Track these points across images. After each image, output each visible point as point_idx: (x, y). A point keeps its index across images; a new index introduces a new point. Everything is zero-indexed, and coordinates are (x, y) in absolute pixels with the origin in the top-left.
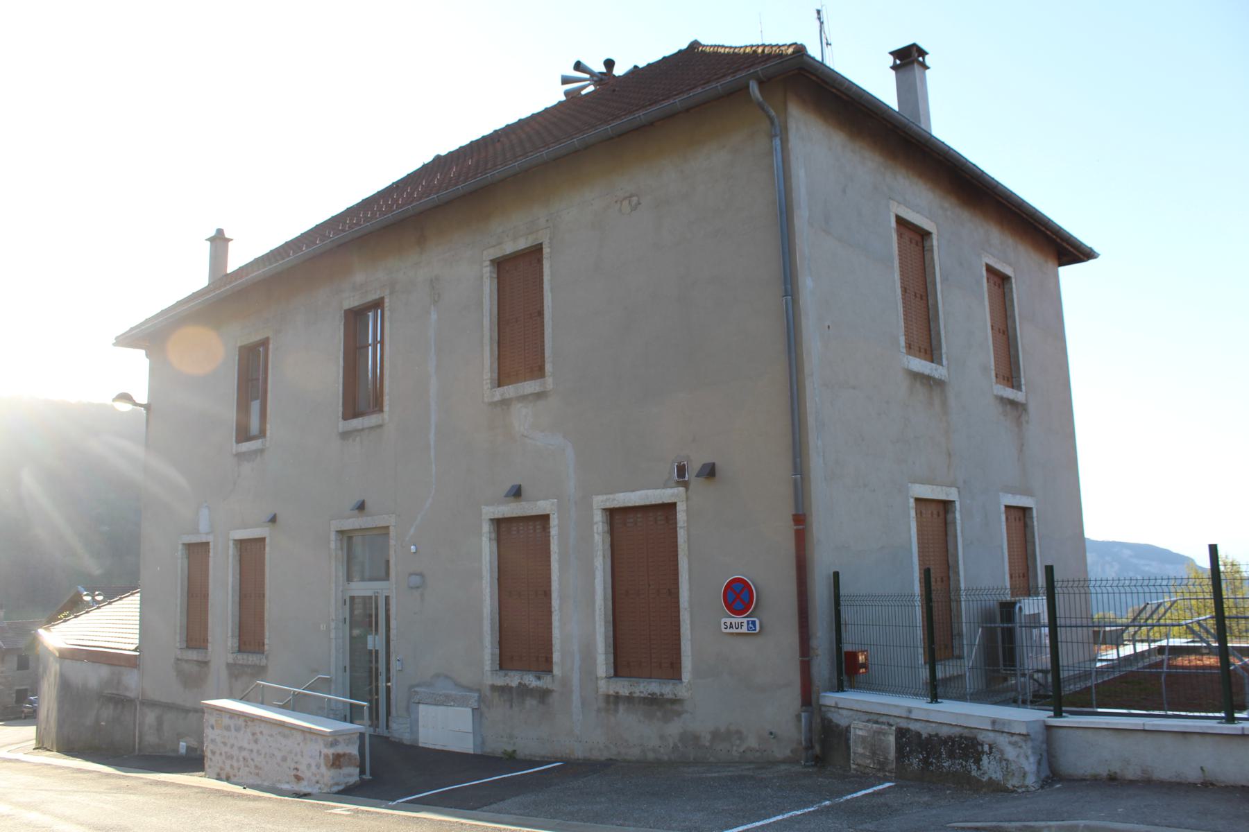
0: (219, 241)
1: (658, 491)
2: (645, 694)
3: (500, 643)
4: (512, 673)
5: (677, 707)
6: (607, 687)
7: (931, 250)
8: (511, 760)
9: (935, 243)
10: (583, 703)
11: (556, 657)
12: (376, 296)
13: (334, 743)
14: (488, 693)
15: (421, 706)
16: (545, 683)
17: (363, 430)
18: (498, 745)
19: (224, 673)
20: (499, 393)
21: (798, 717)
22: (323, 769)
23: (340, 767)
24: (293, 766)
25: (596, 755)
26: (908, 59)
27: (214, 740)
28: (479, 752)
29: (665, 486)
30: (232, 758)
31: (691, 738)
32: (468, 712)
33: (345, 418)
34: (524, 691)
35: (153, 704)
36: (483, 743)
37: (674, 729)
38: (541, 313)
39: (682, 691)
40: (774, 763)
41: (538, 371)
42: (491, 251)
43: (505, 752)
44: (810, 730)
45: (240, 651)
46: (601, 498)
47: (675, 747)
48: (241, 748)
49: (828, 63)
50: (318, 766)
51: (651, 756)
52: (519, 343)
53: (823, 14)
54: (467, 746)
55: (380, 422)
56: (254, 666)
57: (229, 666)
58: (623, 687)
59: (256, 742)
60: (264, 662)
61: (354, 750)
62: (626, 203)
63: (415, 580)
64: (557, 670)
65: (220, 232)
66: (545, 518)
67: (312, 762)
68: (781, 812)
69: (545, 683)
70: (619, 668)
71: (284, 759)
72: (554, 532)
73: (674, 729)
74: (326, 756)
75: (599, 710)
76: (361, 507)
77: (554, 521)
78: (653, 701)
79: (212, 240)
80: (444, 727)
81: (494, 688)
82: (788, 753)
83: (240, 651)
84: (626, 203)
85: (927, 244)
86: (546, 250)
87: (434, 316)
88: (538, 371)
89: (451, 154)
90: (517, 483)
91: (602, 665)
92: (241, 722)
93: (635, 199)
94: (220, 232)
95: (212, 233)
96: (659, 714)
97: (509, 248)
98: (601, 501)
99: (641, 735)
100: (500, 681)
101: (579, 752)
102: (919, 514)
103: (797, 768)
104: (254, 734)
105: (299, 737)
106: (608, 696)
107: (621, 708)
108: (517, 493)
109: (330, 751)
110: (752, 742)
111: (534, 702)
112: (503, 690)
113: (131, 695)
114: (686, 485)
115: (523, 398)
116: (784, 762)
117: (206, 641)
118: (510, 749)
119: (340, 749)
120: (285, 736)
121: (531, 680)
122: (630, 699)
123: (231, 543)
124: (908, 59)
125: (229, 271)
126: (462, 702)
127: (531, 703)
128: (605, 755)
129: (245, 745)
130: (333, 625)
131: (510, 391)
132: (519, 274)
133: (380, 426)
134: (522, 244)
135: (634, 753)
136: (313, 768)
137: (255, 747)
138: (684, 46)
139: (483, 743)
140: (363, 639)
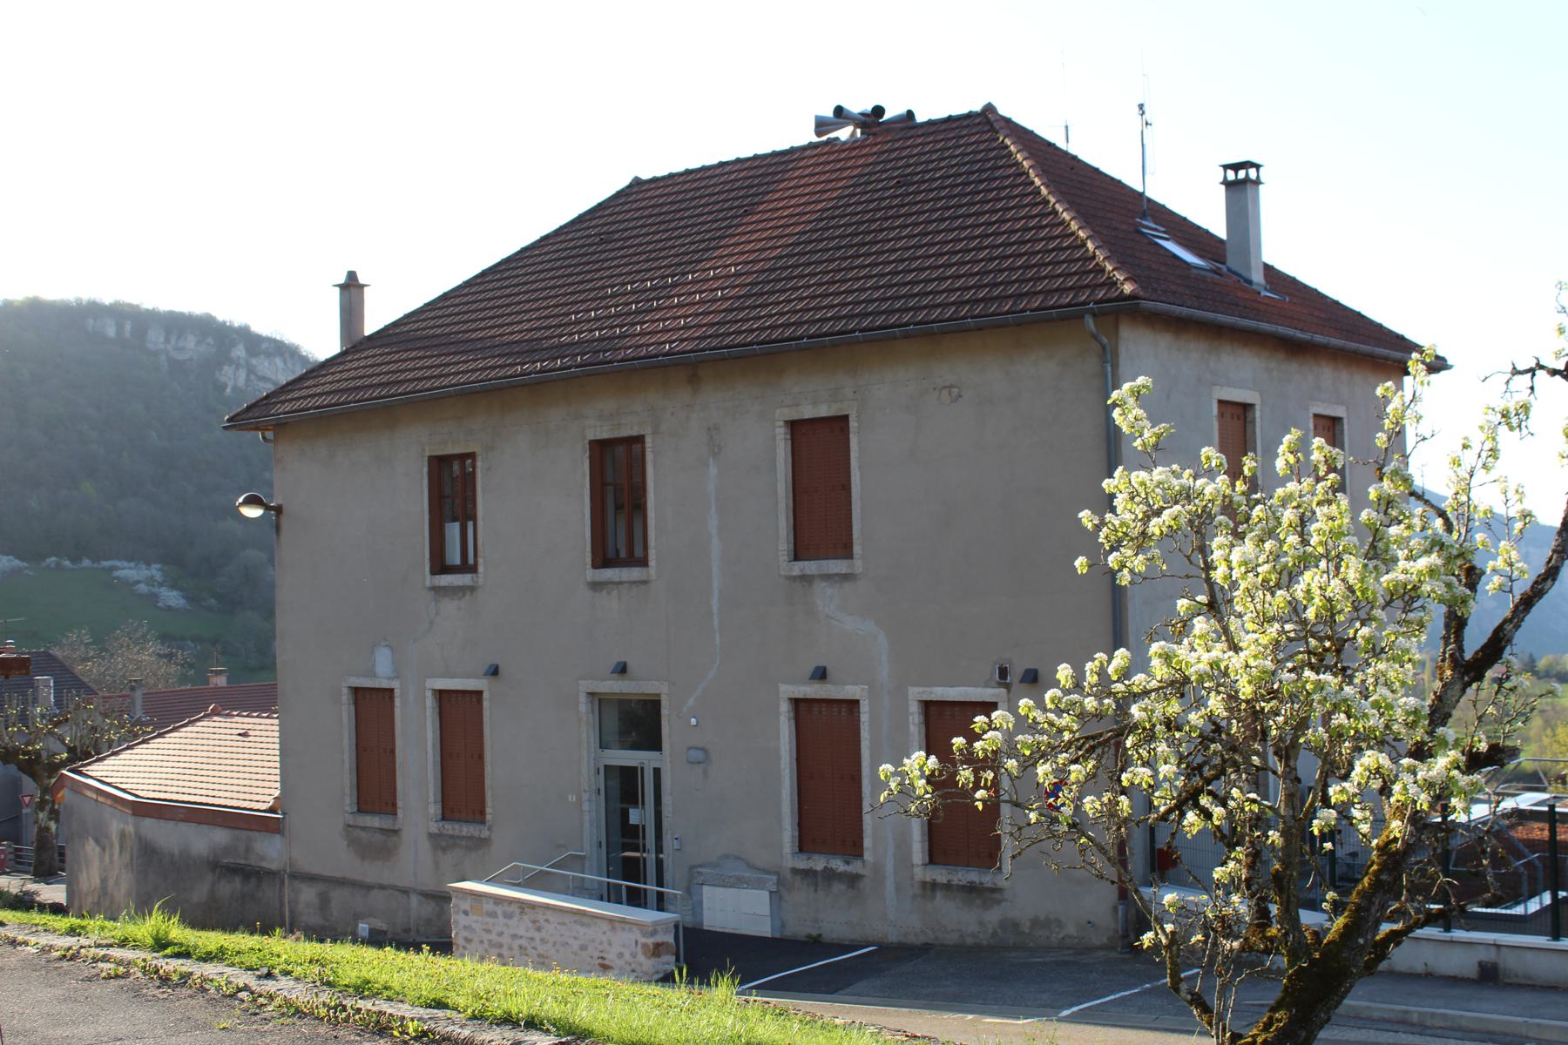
0: (351, 288)
1: (979, 690)
2: (964, 882)
3: (799, 825)
4: (816, 857)
5: (996, 896)
6: (922, 873)
7: (1253, 422)
8: (815, 946)
9: (1258, 414)
10: (898, 889)
11: (867, 842)
12: (634, 432)
13: (654, 933)
14: (789, 876)
15: (705, 888)
16: (855, 867)
17: (621, 583)
18: (799, 927)
19: (425, 846)
20: (798, 568)
21: (1115, 909)
22: (641, 958)
23: (659, 956)
24: (597, 954)
25: (911, 939)
26: (1241, 184)
27: (460, 924)
28: (777, 935)
29: (986, 686)
30: (501, 946)
31: (1012, 925)
32: (766, 894)
33: (595, 566)
34: (830, 875)
35: (312, 878)
36: (783, 926)
37: (993, 916)
38: (847, 488)
39: (1001, 881)
40: (1090, 949)
41: (844, 549)
42: (786, 411)
43: (809, 936)
44: (1126, 921)
45: (444, 818)
46: (917, 689)
47: (995, 934)
48: (514, 936)
49: (1151, 194)
50: (634, 955)
51: (969, 941)
52: (820, 516)
53: (1146, 108)
54: (764, 929)
55: (644, 578)
56: (471, 838)
57: (431, 835)
58: (940, 875)
59: (539, 929)
60: (485, 834)
61: (670, 939)
62: (945, 392)
63: (699, 755)
64: (867, 855)
65: (352, 276)
66: (854, 704)
67: (624, 944)
68: (1112, 993)
69: (855, 867)
70: (935, 856)
71: (583, 948)
72: (864, 718)
73: (993, 916)
74: (645, 946)
75: (914, 897)
76: (622, 669)
77: (865, 708)
78: (971, 889)
79: (344, 288)
80: (738, 909)
81: (795, 871)
82: (1105, 940)
83: (444, 818)
84: (945, 392)
85: (1249, 416)
86: (853, 424)
87: (713, 470)
88: (844, 549)
89: (655, 180)
90: (822, 664)
91: (918, 850)
92: (514, 908)
93: (955, 391)
94: (352, 276)
95: (342, 280)
96: (978, 902)
97: (808, 412)
98: (917, 693)
99: (958, 921)
100: (803, 863)
101: (893, 937)
102: (1221, 415)
103: (1113, 955)
104: (534, 922)
105: (605, 926)
106: (924, 884)
107: (939, 895)
108: (821, 675)
109: (650, 941)
110: (1071, 930)
111: (843, 887)
112: (808, 874)
113: (274, 866)
114: (1008, 687)
115: (828, 577)
116: (1101, 948)
117: (394, 805)
118: (814, 933)
119: (659, 938)
120: (583, 925)
121: (838, 865)
122: (948, 887)
123: (429, 694)
124: (1241, 184)
125: (367, 333)
126: (758, 885)
127: (838, 887)
128: (922, 939)
129: (521, 932)
130: (585, 796)
131: (811, 567)
132: (819, 450)
133: (645, 582)
134: (824, 411)
135: (952, 938)
136: (627, 957)
137: (537, 936)
138: (977, 108)
139: (783, 926)
140: (625, 815)
